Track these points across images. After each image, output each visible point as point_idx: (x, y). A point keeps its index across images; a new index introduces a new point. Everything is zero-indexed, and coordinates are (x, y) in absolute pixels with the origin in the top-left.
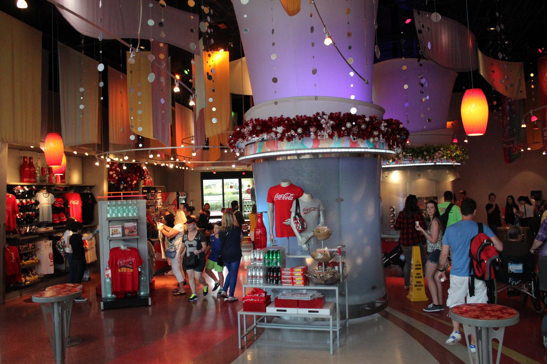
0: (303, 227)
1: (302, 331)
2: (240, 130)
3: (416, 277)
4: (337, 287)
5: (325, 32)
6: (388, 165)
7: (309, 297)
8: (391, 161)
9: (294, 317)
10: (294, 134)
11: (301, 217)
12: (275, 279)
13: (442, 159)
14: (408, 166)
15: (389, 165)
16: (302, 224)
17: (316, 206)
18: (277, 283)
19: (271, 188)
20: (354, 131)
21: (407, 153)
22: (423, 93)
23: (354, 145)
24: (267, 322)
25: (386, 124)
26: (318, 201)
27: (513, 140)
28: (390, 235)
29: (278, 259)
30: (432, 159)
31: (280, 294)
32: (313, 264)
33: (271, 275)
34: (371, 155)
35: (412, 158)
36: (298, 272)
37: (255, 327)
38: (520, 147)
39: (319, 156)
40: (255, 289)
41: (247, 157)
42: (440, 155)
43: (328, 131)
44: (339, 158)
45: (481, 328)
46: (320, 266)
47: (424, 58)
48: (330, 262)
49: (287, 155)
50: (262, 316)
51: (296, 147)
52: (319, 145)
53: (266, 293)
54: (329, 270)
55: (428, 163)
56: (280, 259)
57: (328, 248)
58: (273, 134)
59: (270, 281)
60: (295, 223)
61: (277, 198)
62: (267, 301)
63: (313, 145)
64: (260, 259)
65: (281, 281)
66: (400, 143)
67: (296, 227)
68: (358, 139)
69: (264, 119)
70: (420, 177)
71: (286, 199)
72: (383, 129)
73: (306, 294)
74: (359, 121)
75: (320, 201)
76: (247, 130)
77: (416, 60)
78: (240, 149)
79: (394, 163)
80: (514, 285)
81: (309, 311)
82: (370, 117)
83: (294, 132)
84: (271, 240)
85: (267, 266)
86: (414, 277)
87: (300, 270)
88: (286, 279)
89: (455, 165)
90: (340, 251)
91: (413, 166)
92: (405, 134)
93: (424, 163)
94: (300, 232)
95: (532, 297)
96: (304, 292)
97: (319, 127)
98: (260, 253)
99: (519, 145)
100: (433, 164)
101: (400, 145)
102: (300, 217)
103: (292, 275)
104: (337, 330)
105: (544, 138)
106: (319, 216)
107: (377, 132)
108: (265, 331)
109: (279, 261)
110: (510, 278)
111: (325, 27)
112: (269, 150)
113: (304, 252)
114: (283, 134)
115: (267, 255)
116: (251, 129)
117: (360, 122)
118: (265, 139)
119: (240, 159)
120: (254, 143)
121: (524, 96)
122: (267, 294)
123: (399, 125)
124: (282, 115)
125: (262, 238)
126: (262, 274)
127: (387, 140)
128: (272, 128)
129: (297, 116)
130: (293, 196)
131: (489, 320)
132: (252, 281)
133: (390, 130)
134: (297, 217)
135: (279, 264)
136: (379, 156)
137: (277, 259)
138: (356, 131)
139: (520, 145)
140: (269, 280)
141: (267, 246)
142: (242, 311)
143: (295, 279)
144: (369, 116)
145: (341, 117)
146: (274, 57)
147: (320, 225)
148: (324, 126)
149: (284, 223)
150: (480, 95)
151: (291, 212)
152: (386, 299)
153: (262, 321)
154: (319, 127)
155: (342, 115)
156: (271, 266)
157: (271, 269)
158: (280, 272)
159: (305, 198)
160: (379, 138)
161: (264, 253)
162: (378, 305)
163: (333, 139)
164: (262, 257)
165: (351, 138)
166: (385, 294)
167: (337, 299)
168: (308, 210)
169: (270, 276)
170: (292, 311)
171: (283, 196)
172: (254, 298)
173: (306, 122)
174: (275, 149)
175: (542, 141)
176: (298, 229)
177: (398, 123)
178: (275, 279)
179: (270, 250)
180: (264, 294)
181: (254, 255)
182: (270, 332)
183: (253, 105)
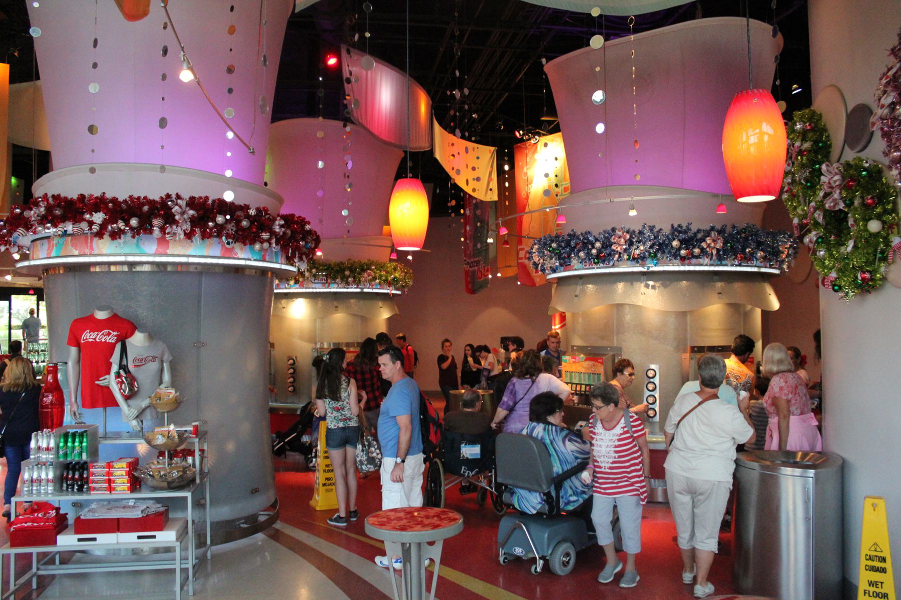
0: (131, 390)
1: (109, 573)
2: (22, 213)
3: (324, 471)
4: (189, 491)
5: (182, 59)
6: (286, 288)
7: (140, 512)
8: (292, 283)
9: (114, 549)
10: (123, 228)
11: (129, 372)
12: (77, 483)
13: (373, 283)
14: (320, 293)
15: (289, 288)
16: (131, 386)
17: (157, 353)
18: (80, 489)
19: (76, 321)
20: (228, 230)
21: (318, 270)
22: (348, 177)
23: (228, 253)
24: (61, 563)
25: (282, 222)
26: (161, 346)
28: (287, 403)
29: (84, 448)
30: (357, 283)
31: (86, 510)
32: (149, 455)
33: (70, 476)
34: (256, 272)
35: (327, 280)
36: (120, 471)
37: (36, 573)
38: (488, 271)
39: (166, 269)
40: (37, 504)
41: (33, 263)
42: (370, 277)
43: (184, 227)
44: (200, 273)
45: (410, 544)
46: (161, 458)
47: (353, 123)
48: (179, 449)
49: (110, 264)
50: (52, 552)
51: (126, 251)
52: (168, 247)
53: (58, 509)
54: (177, 463)
55: (351, 288)
56: (87, 446)
57: (175, 425)
58: (84, 225)
59: (67, 488)
60: (118, 382)
61: (87, 339)
62: (61, 524)
63: (157, 249)
64: (48, 449)
65: (88, 485)
66: (305, 254)
67: (120, 390)
68: (235, 243)
69: (69, 197)
71: (103, 341)
72: (277, 230)
73: (134, 507)
74: (239, 213)
75: (165, 345)
76: (35, 213)
77: (341, 124)
78: (20, 248)
79: (297, 286)
80: (468, 476)
81: (139, 537)
82: (258, 210)
83: (124, 224)
84: (72, 413)
85: (61, 460)
86: (322, 471)
87: (124, 465)
88: (97, 483)
89: (393, 294)
90: (196, 431)
91: (327, 292)
92: (313, 240)
93: (345, 288)
94: (127, 398)
95: (491, 493)
96: (130, 504)
97: (169, 219)
98: (49, 437)
99: (486, 268)
100: (358, 290)
101: (304, 257)
102: (127, 371)
103: (109, 474)
104: (190, 565)
105: (519, 261)
106: (162, 370)
107: (268, 234)
108: (56, 580)
109: (85, 450)
110: (463, 467)
111: (183, 50)
112: (76, 253)
113: (132, 435)
114: (103, 226)
115: (62, 440)
116: (43, 213)
117: (240, 216)
118: (68, 233)
119: (19, 265)
120: (48, 238)
121: (495, 197)
122: (62, 512)
123: (305, 225)
124: (104, 193)
125: (54, 410)
126: (51, 475)
127: (284, 249)
128: (83, 213)
129: (131, 197)
130: (115, 336)
131: (420, 531)
132: (32, 490)
133: (289, 232)
134: (122, 372)
135: (84, 457)
136: (270, 273)
137: (81, 447)
138: (232, 230)
139: (488, 269)
140: (65, 485)
141: (64, 424)
142: (7, 548)
143: (114, 482)
144: (257, 206)
145: (209, 205)
146: (93, 88)
147: (162, 386)
148: (177, 217)
149: (97, 382)
150: (417, 188)
151: (111, 363)
152: (275, 508)
153: (52, 562)
154: (169, 219)
155: (210, 202)
156: (69, 459)
157: (71, 466)
158: (87, 469)
159: (138, 340)
160: (270, 244)
161: (57, 437)
162: (262, 518)
163: (192, 242)
164: (52, 444)
165: (223, 241)
166: (273, 500)
167: (189, 513)
168: (142, 360)
169: (67, 479)
170: (105, 540)
171: (98, 334)
172: (33, 521)
173: (146, 208)
174: (87, 251)
175: (516, 264)
176: (122, 394)
177: (303, 222)
178: (77, 483)
179: (68, 430)
180: (54, 511)
181: (37, 441)
182: (67, 582)
183: (52, 170)
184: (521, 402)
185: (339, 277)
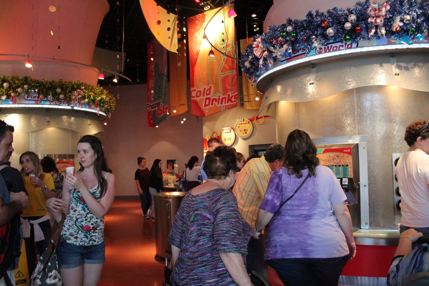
13: (83, 102)
27: (158, 103)
70: (49, 125)
89: (100, 114)
100: (69, 108)
184: (289, 202)
185: (51, 93)
